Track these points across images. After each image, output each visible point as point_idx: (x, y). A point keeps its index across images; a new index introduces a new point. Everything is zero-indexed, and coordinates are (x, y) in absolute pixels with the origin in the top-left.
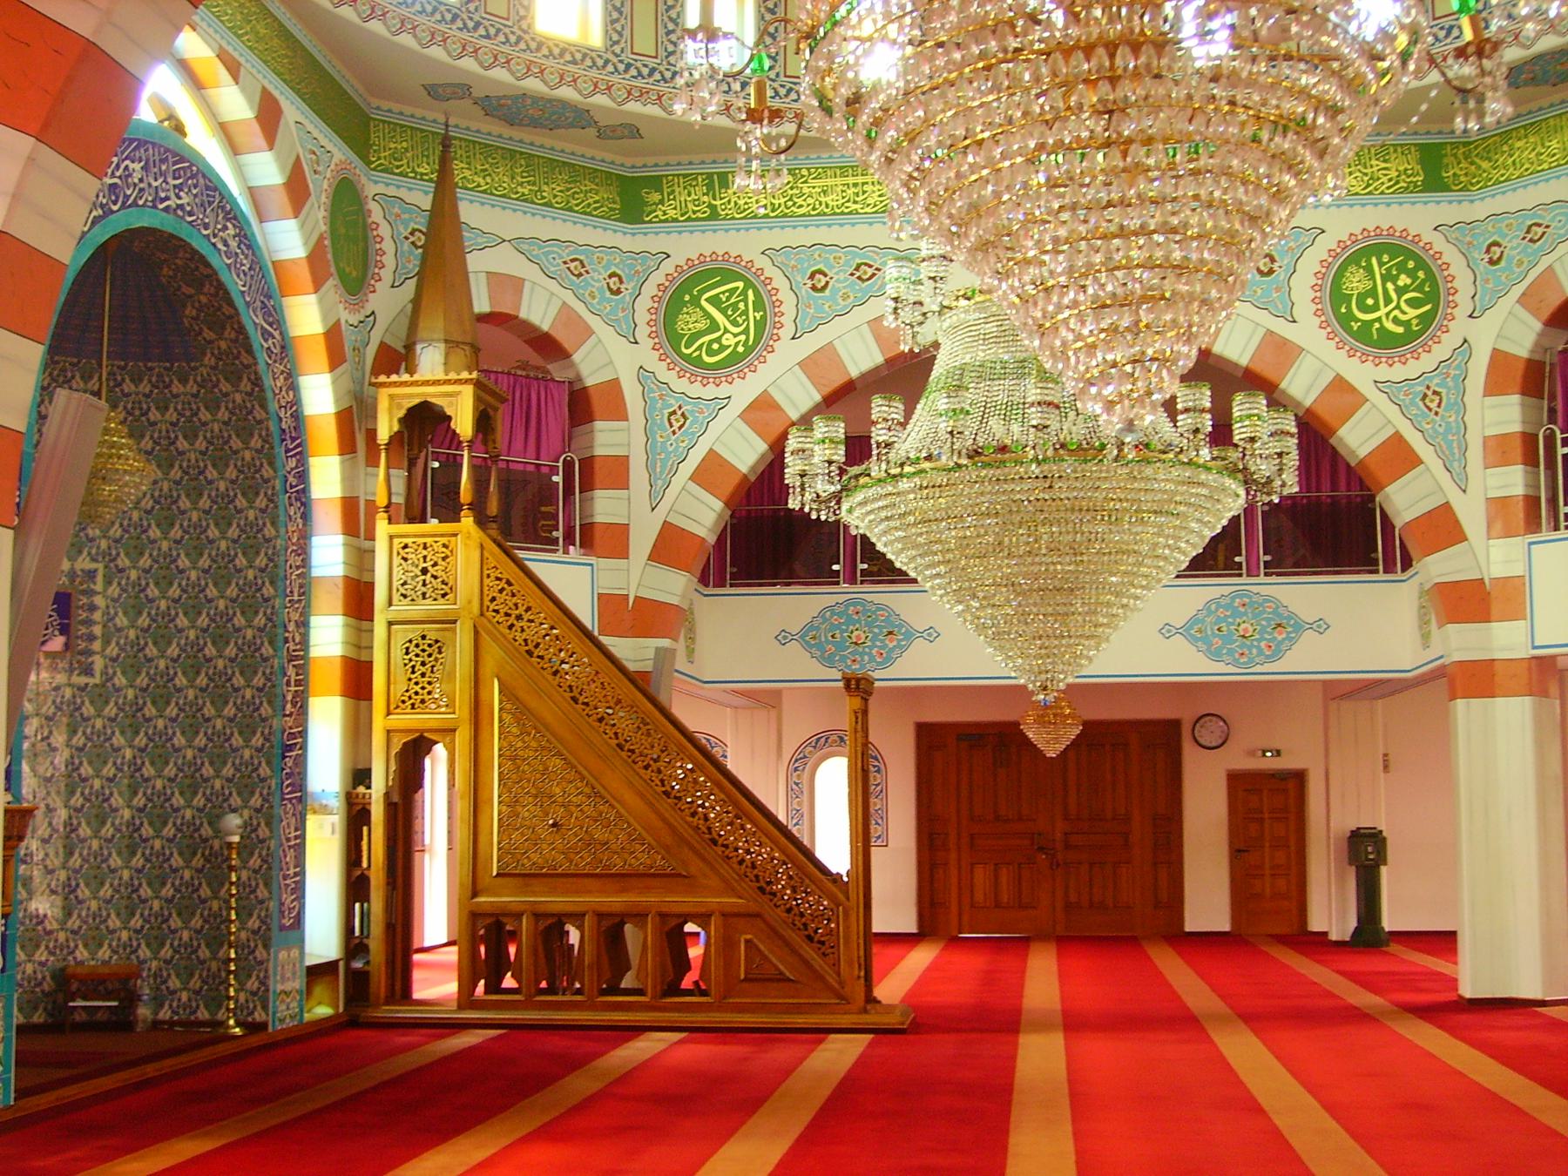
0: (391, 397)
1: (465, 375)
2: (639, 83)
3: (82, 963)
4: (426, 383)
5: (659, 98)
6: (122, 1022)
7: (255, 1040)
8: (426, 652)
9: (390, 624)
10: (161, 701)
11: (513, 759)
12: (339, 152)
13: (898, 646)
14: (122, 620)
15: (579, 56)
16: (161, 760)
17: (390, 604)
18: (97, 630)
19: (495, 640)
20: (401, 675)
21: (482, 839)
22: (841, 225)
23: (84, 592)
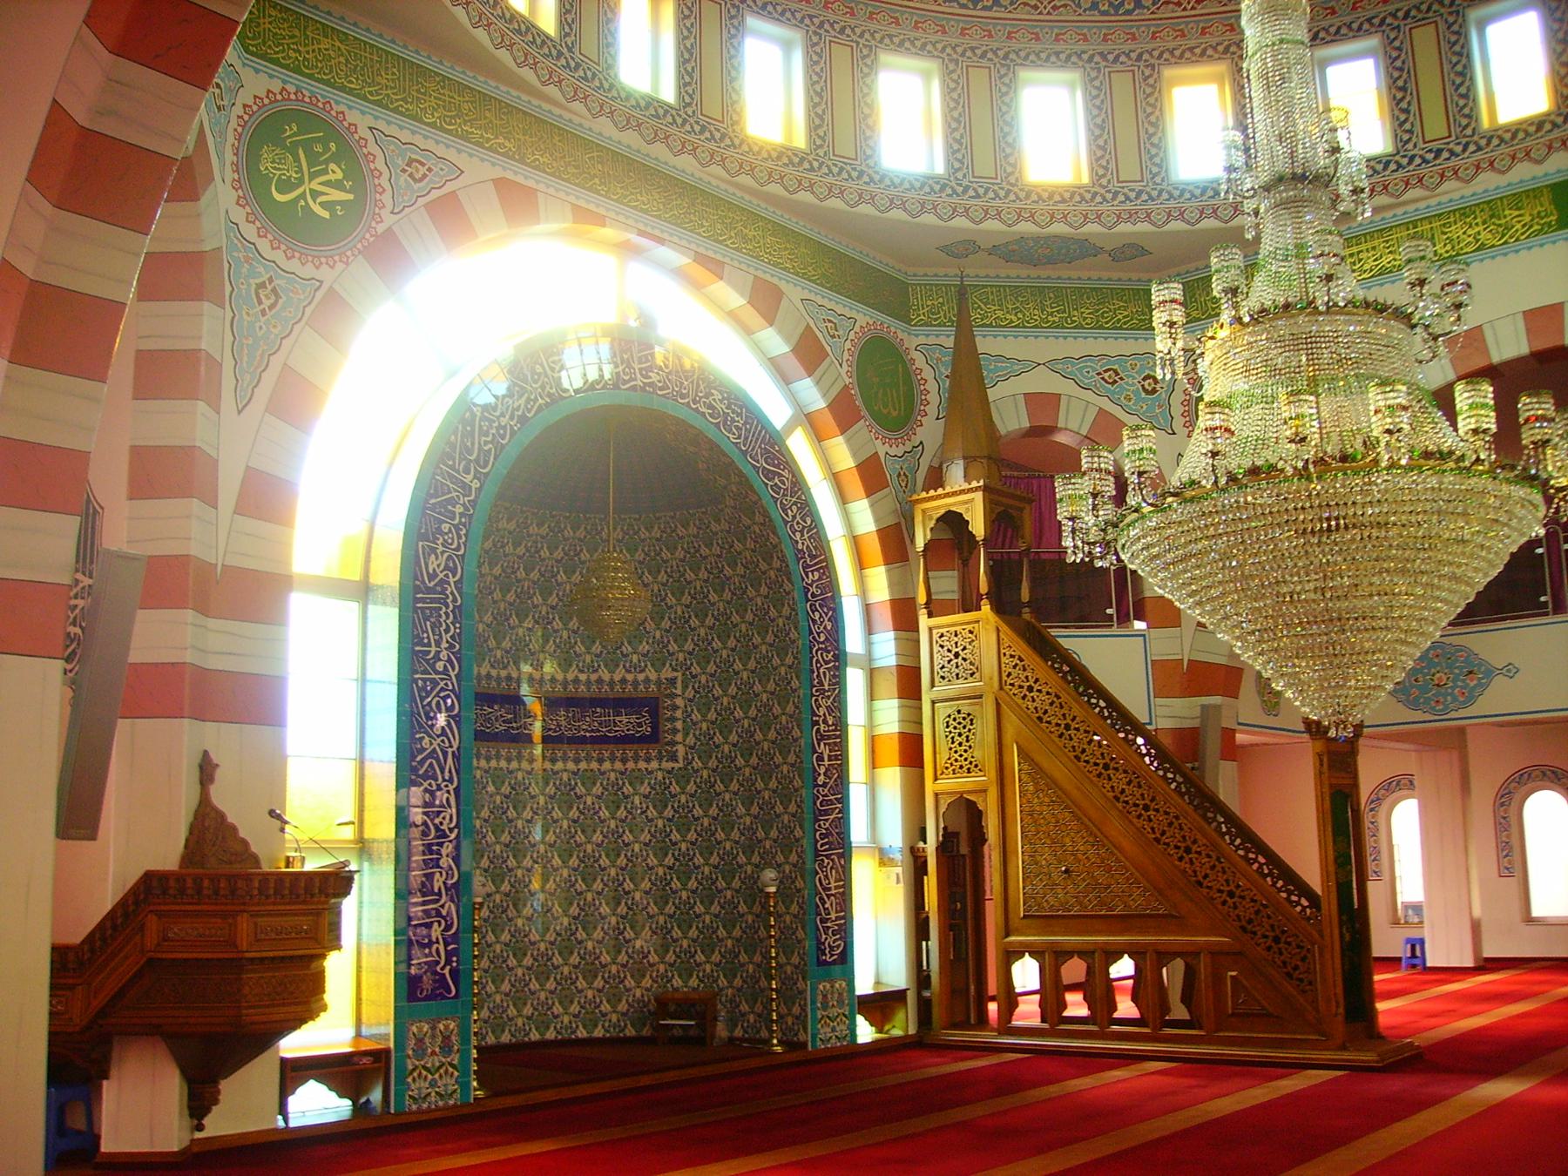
0: (924, 511)
1: (974, 484)
2: (1128, 206)
3: (676, 990)
4: (954, 494)
5: (1148, 215)
6: (700, 1039)
7: (796, 1056)
9: (933, 703)
10: (727, 779)
12: (864, 317)
13: (1479, 685)
14: (696, 716)
15: (1075, 194)
17: (933, 686)
18: (679, 725)
22: (482, 160)
23: (667, 696)
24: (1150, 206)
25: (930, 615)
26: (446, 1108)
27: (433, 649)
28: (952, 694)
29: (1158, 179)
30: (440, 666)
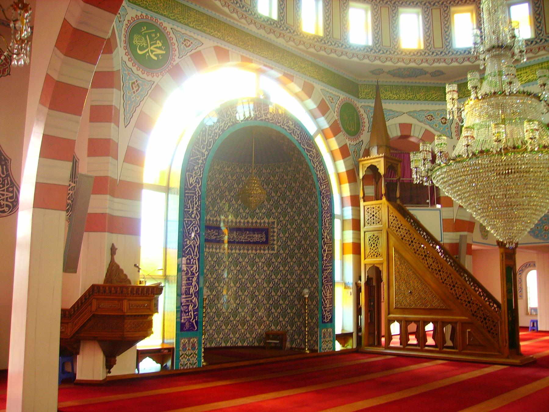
1: (381, 155)
2: (437, 57)
3: (273, 330)
4: (374, 159)
6: (280, 347)
7: (314, 354)
8: (375, 240)
9: (365, 232)
11: (399, 272)
14: (281, 235)
15: (418, 52)
16: (276, 274)
17: (365, 226)
18: (275, 238)
19: (392, 235)
20: (368, 247)
21: (391, 297)
24: (445, 57)
25: (364, 201)
26: (193, 368)
27: (191, 210)
28: (371, 229)
29: (448, 47)
30: (193, 216)
